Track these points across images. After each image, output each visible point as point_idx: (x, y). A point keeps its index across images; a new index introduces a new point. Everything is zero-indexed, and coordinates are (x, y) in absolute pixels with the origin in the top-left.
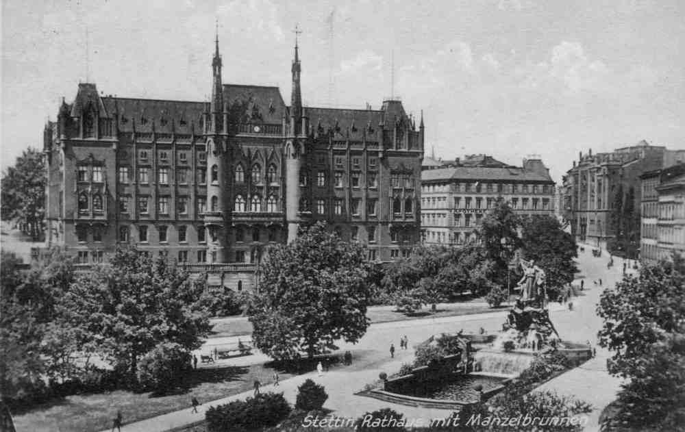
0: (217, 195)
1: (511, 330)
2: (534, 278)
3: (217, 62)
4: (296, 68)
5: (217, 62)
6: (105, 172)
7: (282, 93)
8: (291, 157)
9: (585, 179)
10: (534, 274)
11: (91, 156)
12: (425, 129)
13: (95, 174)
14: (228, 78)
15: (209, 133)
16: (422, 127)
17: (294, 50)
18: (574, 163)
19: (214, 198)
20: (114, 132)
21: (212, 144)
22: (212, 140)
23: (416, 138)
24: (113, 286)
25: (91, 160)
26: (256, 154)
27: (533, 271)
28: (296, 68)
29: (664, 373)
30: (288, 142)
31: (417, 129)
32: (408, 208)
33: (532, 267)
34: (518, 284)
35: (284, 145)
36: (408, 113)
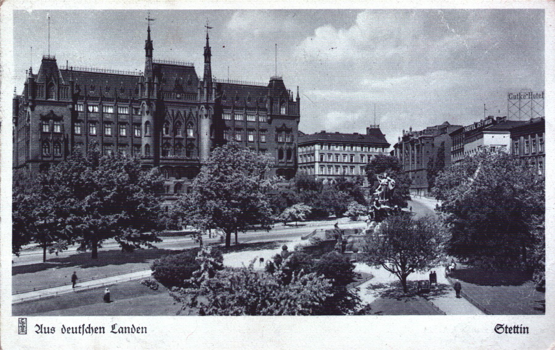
0: (149, 144)
1: (409, 130)
2: (387, 185)
3: (149, 47)
4: (208, 54)
5: (149, 47)
6: (63, 125)
7: (196, 71)
8: (204, 117)
9: (407, 149)
10: (388, 183)
11: (284, 125)
12: (301, 100)
13: (55, 127)
14: (158, 56)
15: (143, 97)
16: (298, 99)
17: (206, 40)
18: (399, 139)
19: (147, 146)
20: (70, 96)
21: (146, 106)
22: (145, 102)
23: (294, 107)
24: (48, 71)
25: (51, 116)
26: (178, 114)
27: (386, 180)
28: (208, 54)
29: (518, 197)
30: (143, 102)
31: (295, 100)
32: (289, 157)
33: (386, 178)
34: (376, 190)
35: (199, 108)
36: (287, 88)
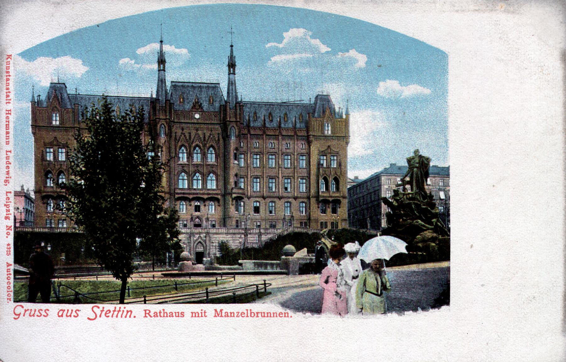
4: (232, 65)
28: (232, 65)
